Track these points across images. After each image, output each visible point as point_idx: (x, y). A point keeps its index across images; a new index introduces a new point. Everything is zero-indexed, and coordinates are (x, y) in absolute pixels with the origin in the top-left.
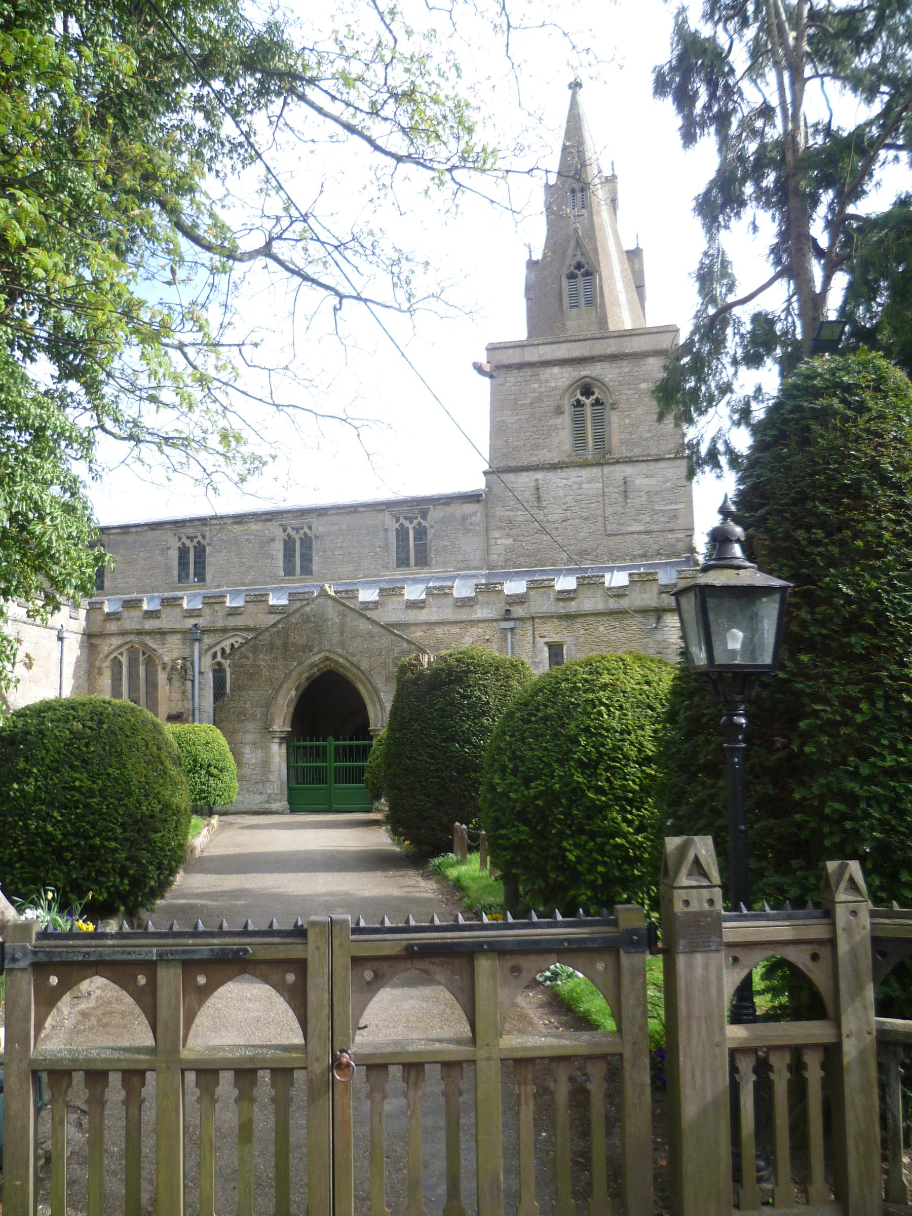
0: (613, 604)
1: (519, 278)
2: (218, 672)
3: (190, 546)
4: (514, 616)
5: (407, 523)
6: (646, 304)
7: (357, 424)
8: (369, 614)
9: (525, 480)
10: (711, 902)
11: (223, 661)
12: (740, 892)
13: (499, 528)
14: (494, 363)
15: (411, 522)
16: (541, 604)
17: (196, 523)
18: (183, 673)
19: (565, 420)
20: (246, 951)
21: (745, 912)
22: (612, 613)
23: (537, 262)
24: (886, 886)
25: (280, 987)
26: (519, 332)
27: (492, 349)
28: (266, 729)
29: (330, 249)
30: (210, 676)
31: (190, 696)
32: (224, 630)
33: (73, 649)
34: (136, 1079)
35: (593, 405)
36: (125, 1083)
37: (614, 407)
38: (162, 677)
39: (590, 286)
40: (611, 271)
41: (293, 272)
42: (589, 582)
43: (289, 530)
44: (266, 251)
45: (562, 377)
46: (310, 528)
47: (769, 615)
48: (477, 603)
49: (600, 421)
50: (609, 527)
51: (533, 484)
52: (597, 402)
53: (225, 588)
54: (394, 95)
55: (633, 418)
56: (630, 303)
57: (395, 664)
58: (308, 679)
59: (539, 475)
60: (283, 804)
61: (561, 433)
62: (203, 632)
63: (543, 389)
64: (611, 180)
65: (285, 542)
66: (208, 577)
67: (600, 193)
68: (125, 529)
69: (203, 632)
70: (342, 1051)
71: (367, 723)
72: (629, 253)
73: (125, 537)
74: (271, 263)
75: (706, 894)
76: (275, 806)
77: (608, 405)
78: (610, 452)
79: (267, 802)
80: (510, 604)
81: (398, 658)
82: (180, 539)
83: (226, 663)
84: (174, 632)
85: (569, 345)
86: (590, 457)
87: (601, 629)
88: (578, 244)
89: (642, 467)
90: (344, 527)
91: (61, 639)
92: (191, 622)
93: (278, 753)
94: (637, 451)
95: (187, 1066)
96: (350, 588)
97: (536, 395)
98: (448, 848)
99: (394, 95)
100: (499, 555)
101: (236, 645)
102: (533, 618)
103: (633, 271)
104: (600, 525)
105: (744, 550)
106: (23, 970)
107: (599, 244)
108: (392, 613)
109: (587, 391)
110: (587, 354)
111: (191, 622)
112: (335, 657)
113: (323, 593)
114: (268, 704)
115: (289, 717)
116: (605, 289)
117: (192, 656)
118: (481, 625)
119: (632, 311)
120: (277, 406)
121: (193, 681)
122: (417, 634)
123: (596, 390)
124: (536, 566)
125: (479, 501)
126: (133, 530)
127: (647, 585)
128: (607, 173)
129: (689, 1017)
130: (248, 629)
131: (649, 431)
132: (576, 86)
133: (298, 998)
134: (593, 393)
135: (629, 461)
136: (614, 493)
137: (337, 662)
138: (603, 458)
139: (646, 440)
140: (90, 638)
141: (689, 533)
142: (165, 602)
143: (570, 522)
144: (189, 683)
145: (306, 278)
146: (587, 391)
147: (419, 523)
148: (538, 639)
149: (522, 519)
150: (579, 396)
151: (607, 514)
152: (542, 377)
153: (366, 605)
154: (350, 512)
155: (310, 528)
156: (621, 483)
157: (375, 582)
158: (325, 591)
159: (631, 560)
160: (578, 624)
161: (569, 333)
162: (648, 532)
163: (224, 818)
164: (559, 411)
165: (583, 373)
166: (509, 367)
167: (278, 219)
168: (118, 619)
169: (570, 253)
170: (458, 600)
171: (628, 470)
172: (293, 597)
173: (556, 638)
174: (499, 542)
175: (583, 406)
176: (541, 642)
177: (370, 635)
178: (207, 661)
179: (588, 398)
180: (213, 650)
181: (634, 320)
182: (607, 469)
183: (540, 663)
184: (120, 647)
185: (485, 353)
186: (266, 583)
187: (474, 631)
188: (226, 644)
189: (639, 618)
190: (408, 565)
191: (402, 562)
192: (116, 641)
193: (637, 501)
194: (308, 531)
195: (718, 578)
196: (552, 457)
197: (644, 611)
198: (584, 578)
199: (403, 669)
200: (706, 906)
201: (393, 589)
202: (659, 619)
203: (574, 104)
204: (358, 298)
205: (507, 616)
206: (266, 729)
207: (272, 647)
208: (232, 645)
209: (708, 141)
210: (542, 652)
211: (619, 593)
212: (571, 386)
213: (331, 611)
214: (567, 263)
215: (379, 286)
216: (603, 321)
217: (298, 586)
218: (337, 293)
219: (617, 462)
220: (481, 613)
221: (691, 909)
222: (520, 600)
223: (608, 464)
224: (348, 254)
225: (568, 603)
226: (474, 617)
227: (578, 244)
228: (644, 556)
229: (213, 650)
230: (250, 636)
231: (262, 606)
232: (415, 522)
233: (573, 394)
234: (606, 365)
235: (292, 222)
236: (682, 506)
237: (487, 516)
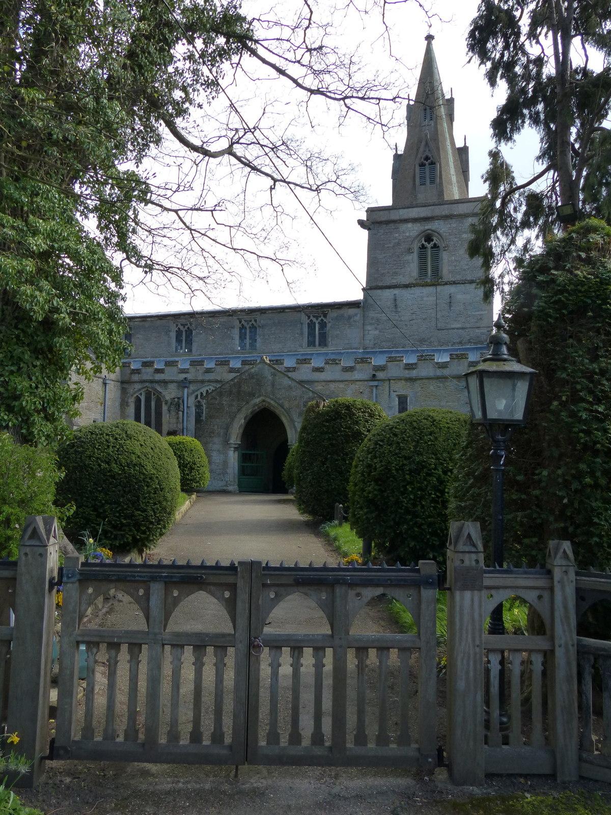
0: (439, 372)
2: (198, 406)
3: (184, 327)
5: (314, 320)
6: (470, 183)
7: (282, 262)
8: (290, 374)
9: (388, 294)
10: (477, 561)
11: (201, 401)
12: (497, 556)
15: (317, 319)
16: (394, 371)
17: (186, 316)
18: (177, 405)
19: (414, 257)
20: (202, 577)
21: (498, 568)
22: (437, 378)
23: (401, 155)
24: (586, 559)
25: (220, 598)
26: (386, 200)
27: (370, 211)
28: (226, 443)
29: (267, 150)
30: (193, 409)
31: (181, 421)
32: (202, 382)
33: (113, 391)
34: (136, 650)
35: (432, 248)
36: (130, 651)
37: (446, 248)
38: (165, 408)
39: (433, 171)
41: (245, 164)
43: (243, 322)
44: (230, 151)
45: (413, 230)
46: (256, 321)
47: (522, 389)
48: (356, 370)
49: (436, 258)
52: (435, 246)
53: (204, 356)
54: (309, 50)
55: (455, 260)
56: (458, 182)
57: (305, 406)
58: (252, 413)
60: (234, 487)
61: (412, 265)
62: (190, 382)
64: (451, 101)
65: (241, 329)
66: (194, 349)
67: (443, 111)
68: (144, 318)
69: (190, 382)
70: (255, 638)
71: (287, 441)
72: (459, 149)
73: (143, 323)
74: (233, 160)
75: (474, 556)
76: (230, 488)
77: (441, 248)
78: (441, 278)
79: (226, 486)
80: (376, 371)
81: (307, 402)
82: (177, 325)
83: (204, 402)
84: (172, 382)
86: (429, 281)
87: (432, 388)
88: (427, 144)
90: (276, 321)
91: (105, 384)
92: (183, 376)
93: (233, 458)
95: (166, 642)
96: (279, 358)
97: (397, 241)
98: (331, 519)
99: (309, 50)
100: (370, 340)
101: (210, 391)
103: (462, 161)
105: (509, 349)
106: (72, 583)
108: (305, 373)
109: (429, 239)
110: (430, 215)
111: (183, 376)
112: (269, 400)
113: (263, 361)
114: (227, 428)
115: (240, 435)
117: (183, 397)
118: (358, 383)
119: (460, 187)
120: (235, 249)
121: (183, 412)
122: (319, 388)
123: (435, 238)
124: (393, 348)
125: (359, 307)
126: (149, 319)
128: (448, 97)
129: (461, 629)
130: (217, 381)
131: (467, 265)
132: (429, 38)
133: (231, 606)
134: (432, 240)
137: (269, 403)
138: (437, 280)
139: (464, 270)
140: (124, 383)
142: (168, 364)
143: (414, 321)
144: (181, 413)
145: (254, 168)
146: (429, 239)
147: (322, 320)
153: (288, 369)
154: (281, 312)
155: (256, 321)
157: (295, 355)
158: (264, 360)
162: (463, 328)
163: (199, 495)
164: (409, 251)
165: (426, 228)
167: (237, 130)
168: (139, 373)
169: (421, 149)
170: (437, 363)
172: (244, 363)
174: (370, 332)
175: (426, 248)
176: (394, 395)
177: (290, 387)
178: (192, 400)
179: (429, 243)
180: (196, 394)
181: (460, 193)
182: (439, 288)
183: (392, 407)
184: (140, 390)
186: (228, 354)
187: (353, 386)
188: (204, 390)
189: (455, 381)
190: (314, 346)
191: (311, 343)
192: (137, 386)
194: (254, 323)
195: (493, 367)
196: (406, 280)
197: (458, 377)
199: (311, 409)
200: (474, 563)
201: (305, 360)
204: (284, 181)
206: (226, 443)
207: (231, 393)
208: (207, 391)
209: (503, 86)
211: (444, 366)
212: (419, 235)
213: (267, 372)
214: (419, 156)
215: (298, 174)
216: (441, 193)
217: (249, 357)
218: (273, 178)
219: (446, 284)
220: (356, 375)
221: (464, 565)
222: (382, 368)
223: (439, 285)
224: (280, 154)
226: (353, 378)
227: (427, 144)
228: (460, 343)
229: (196, 394)
230: (219, 385)
231: (226, 367)
232: (320, 319)
233: (420, 241)
234: (441, 222)
235: (245, 133)
237: (364, 316)
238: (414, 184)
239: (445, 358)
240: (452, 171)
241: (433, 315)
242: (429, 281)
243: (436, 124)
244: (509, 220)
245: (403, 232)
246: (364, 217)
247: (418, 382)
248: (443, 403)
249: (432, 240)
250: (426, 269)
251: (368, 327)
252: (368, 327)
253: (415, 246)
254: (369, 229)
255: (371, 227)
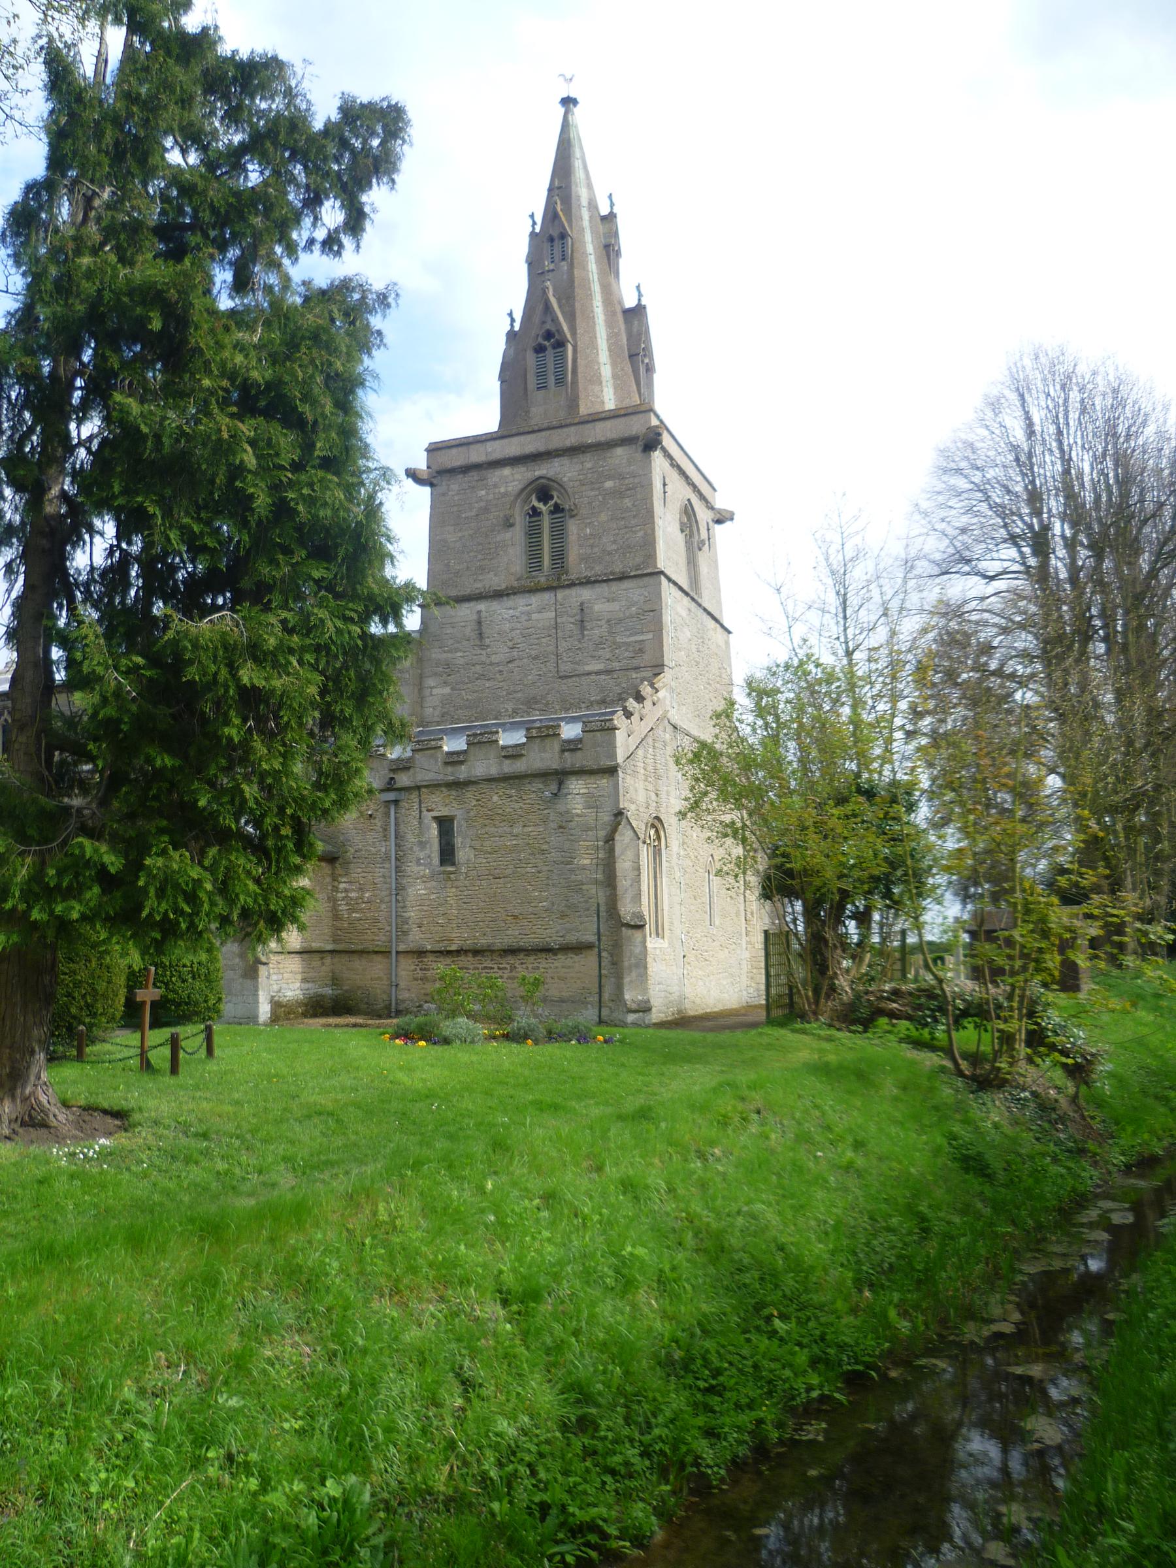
0: (509, 767)
1: (522, 247)
4: (398, 785)
9: (466, 612)
13: (436, 674)
14: (435, 467)
19: (517, 535)
35: (552, 513)
40: (593, 338)
42: (481, 741)
45: (513, 479)
49: (559, 533)
50: (562, 667)
51: (475, 617)
52: (557, 509)
56: (615, 376)
59: (482, 606)
61: (511, 551)
63: (491, 497)
85: (522, 438)
86: (543, 579)
87: (495, 798)
89: (603, 589)
94: (598, 569)
97: (482, 504)
100: (434, 708)
102: (418, 788)
104: (551, 665)
107: (578, 305)
109: (544, 494)
110: (542, 449)
116: (581, 362)
123: (555, 494)
124: (477, 720)
127: (548, 741)
131: (614, 542)
135: (588, 582)
136: (568, 623)
138: (559, 582)
139: (610, 553)
141: (657, 670)
143: (516, 663)
146: (544, 494)
148: (425, 813)
149: (461, 661)
150: (535, 503)
151: (561, 650)
152: (490, 482)
156: (576, 610)
159: (587, 708)
160: (469, 794)
161: (533, 422)
162: (608, 672)
164: (508, 524)
165: (537, 473)
166: (451, 472)
171: (585, 594)
173: (444, 812)
174: (435, 691)
182: (561, 594)
183: (426, 843)
185: (424, 455)
189: (538, 785)
193: (597, 632)
197: (543, 775)
198: (475, 735)
202: (561, 783)
203: (566, 125)
205: (390, 786)
210: (429, 828)
211: (514, 753)
216: (573, 403)
219: (572, 585)
222: (402, 766)
225: (457, 768)
233: (527, 500)
234: (565, 461)
236: (650, 636)
238: (526, 389)
239: (517, 737)
240: (604, 356)
241: (551, 648)
242: (543, 579)
243: (571, 266)
244: (125, 299)
245: (495, 486)
246: (421, 463)
247: (472, 788)
248: (517, 830)
249: (552, 498)
250: (540, 557)
251: (431, 682)
252: (431, 682)
253: (517, 510)
254: (432, 485)
255: (435, 481)
